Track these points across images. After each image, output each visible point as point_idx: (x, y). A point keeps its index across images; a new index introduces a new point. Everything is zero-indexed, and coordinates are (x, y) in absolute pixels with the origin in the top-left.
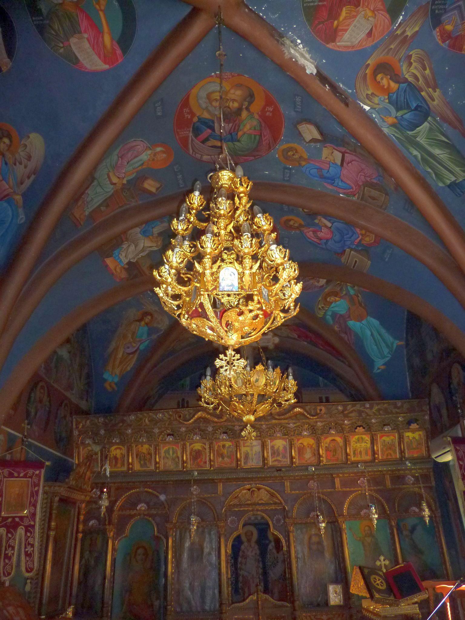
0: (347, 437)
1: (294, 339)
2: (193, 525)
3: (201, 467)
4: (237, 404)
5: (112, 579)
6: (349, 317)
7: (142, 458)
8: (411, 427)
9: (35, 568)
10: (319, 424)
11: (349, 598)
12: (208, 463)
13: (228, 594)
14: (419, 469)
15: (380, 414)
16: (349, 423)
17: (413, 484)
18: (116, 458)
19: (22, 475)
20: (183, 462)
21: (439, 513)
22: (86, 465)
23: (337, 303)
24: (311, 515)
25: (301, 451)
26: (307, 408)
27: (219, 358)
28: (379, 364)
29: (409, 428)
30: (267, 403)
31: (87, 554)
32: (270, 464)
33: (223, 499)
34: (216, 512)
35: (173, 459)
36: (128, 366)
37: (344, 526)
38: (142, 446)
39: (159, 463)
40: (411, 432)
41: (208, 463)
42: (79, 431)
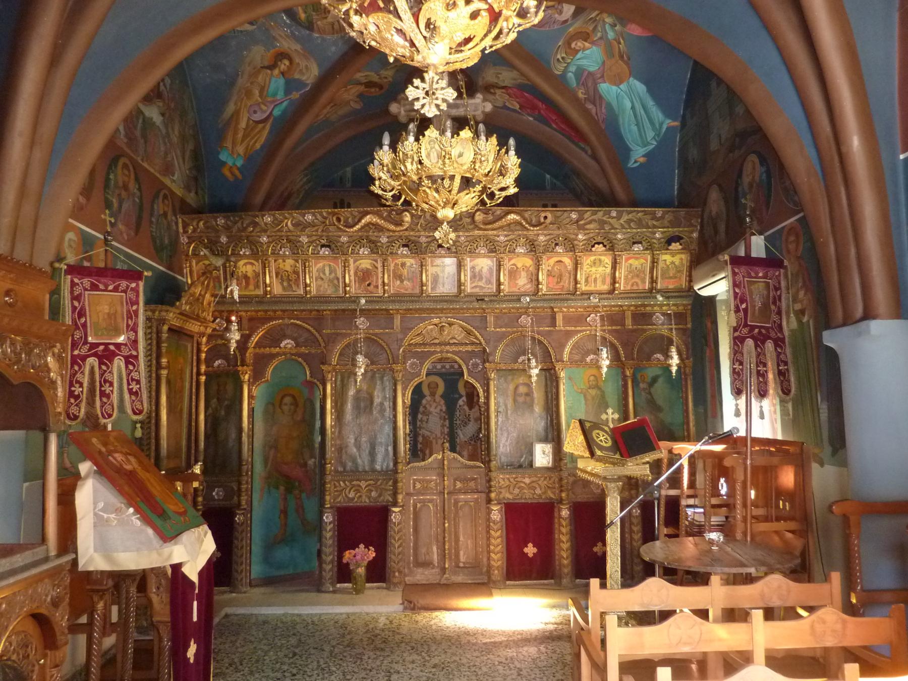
0: (580, 257)
1: (514, 111)
2: (360, 367)
3: (371, 293)
4: (428, 190)
5: (251, 433)
6: (602, 76)
7: (285, 278)
8: (670, 247)
9: (145, 410)
10: (542, 238)
11: (561, 460)
12: (380, 287)
13: (405, 452)
14: (673, 305)
15: (631, 228)
16: (584, 238)
17: (663, 324)
18: (246, 277)
19: (111, 288)
20: (345, 285)
21: (689, 362)
22: (203, 283)
23: (587, 52)
24: (520, 360)
25: (513, 274)
26: (527, 215)
27: (412, 84)
28: (638, 155)
29: (667, 249)
30: (474, 192)
31: (214, 402)
32: (469, 290)
33: (400, 336)
34: (392, 354)
35: (331, 281)
36: (255, 142)
37: (562, 374)
38: (284, 261)
39: (310, 285)
40: (671, 254)
41: (380, 287)
42: (189, 238)
